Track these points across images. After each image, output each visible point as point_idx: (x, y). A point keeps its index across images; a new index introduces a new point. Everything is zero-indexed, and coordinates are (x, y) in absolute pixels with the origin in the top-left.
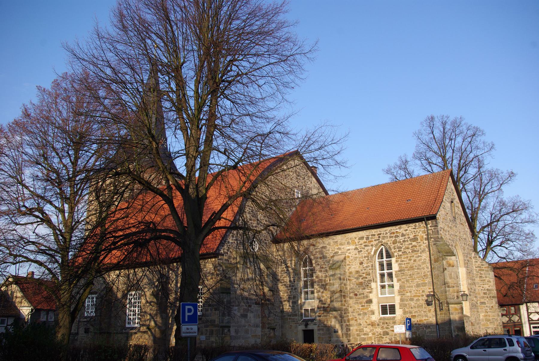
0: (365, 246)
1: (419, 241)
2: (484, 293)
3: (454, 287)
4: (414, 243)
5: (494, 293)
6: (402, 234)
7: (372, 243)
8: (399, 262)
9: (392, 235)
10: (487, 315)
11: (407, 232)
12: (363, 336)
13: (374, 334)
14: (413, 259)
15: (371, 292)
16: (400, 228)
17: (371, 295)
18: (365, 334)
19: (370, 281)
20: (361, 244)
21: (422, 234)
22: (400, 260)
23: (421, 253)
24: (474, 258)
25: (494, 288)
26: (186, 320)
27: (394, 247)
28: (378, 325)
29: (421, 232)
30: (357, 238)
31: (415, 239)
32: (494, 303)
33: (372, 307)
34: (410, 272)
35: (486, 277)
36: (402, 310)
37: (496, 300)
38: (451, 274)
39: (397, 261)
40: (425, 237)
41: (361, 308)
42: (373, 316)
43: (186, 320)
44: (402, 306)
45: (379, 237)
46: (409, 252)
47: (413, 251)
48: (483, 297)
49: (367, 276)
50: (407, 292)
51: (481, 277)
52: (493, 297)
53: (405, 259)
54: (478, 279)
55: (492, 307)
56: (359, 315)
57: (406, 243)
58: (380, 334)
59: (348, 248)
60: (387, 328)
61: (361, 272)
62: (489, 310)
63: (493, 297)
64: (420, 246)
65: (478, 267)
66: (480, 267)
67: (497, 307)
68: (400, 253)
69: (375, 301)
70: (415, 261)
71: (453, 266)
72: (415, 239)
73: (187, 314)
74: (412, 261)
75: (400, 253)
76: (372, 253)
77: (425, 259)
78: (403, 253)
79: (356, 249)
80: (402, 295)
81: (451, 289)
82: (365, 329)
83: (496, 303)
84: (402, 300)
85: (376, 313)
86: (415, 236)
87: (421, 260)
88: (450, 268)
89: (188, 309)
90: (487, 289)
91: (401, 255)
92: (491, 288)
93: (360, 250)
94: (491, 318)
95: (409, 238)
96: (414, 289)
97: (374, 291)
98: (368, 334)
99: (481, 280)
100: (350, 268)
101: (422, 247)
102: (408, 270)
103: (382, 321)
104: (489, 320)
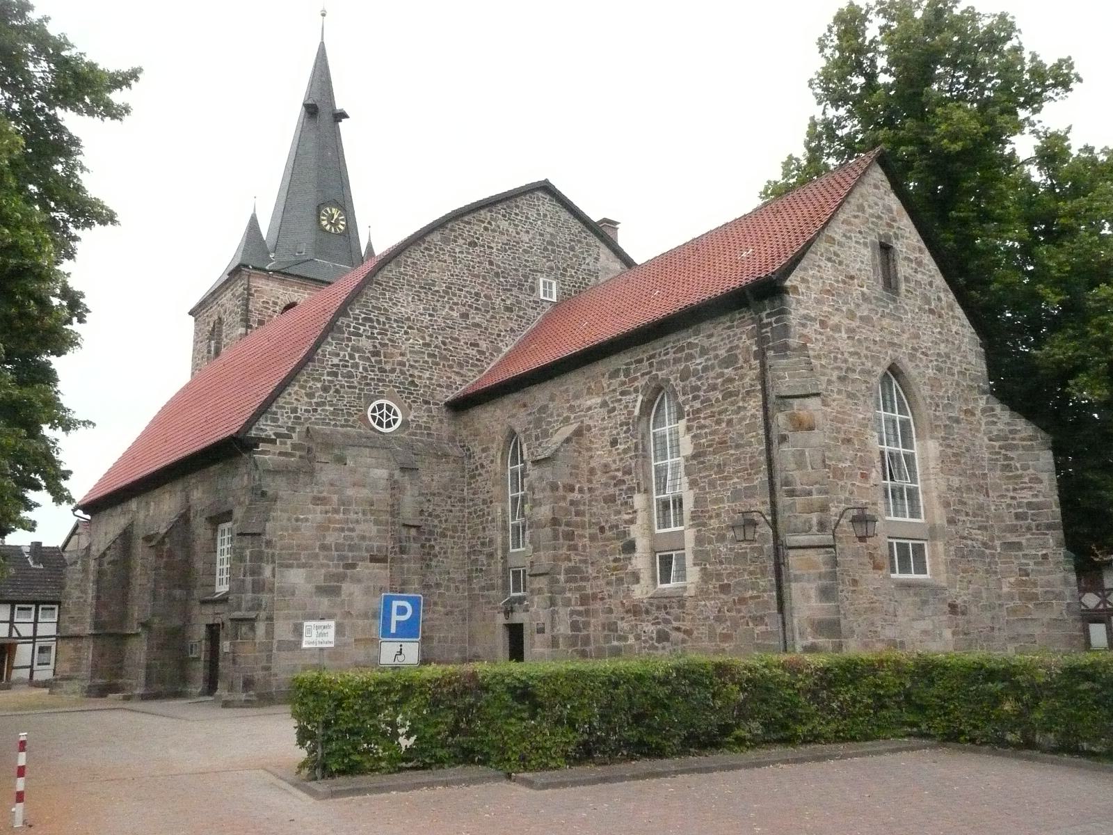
0: (623, 393)
1: (741, 362)
2: (1018, 516)
3: (810, 493)
4: (729, 372)
5: (1054, 512)
6: (702, 347)
7: (636, 384)
8: (695, 431)
9: (679, 355)
10: (1024, 583)
11: (714, 340)
12: (615, 643)
13: (638, 638)
14: (725, 417)
15: (632, 521)
16: (697, 333)
17: (632, 527)
18: (620, 638)
19: (631, 489)
20: (614, 391)
21: (748, 342)
22: (695, 424)
23: (743, 400)
24: (984, 411)
25: (1054, 497)
26: (393, 630)
27: (683, 388)
28: (647, 612)
29: (744, 337)
30: (607, 376)
31: (730, 361)
32: (1053, 541)
33: (633, 561)
34: (718, 459)
35: (1025, 468)
36: (698, 568)
37: (1060, 534)
38: (802, 453)
39: (689, 429)
40: (755, 348)
41: (612, 565)
42: (636, 586)
43: (393, 630)
44: (701, 558)
45: (651, 365)
46: (717, 400)
47: (728, 395)
48: (1013, 529)
49: (626, 477)
50: (711, 517)
51: (1007, 467)
52: (1049, 527)
53: (708, 422)
54: (998, 473)
55: (1045, 556)
56: (608, 584)
57: (712, 374)
58: (652, 639)
59: (589, 403)
60: (667, 621)
61: (614, 467)
62: (1031, 566)
63: (1049, 527)
64: (742, 378)
65: (998, 438)
66: (1006, 439)
67: (1062, 558)
68: (697, 405)
69: (642, 544)
70: (730, 422)
71: (811, 428)
72: (730, 361)
73: (395, 618)
74: (724, 425)
75: (697, 405)
76: (637, 412)
77: (753, 416)
78: (702, 402)
79: (604, 404)
80: (698, 525)
81: (799, 500)
82: (619, 622)
83: (1059, 545)
84: (699, 540)
85: (645, 576)
86: (731, 349)
87: (743, 419)
88: (799, 434)
89: (398, 607)
90: (1029, 505)
91: (698, 411)
92: (1041, 499)
93: (611, 405)
94: (1039, 590)
95: (716, 357)
96: (726, 505)
97: (641, 518)
98: (625, 638)
99: (1009, 478)
100: (591, 457)
101: (747, 380)
102: (715, 453)
103: (656, 601)
104: (1033, 597)
